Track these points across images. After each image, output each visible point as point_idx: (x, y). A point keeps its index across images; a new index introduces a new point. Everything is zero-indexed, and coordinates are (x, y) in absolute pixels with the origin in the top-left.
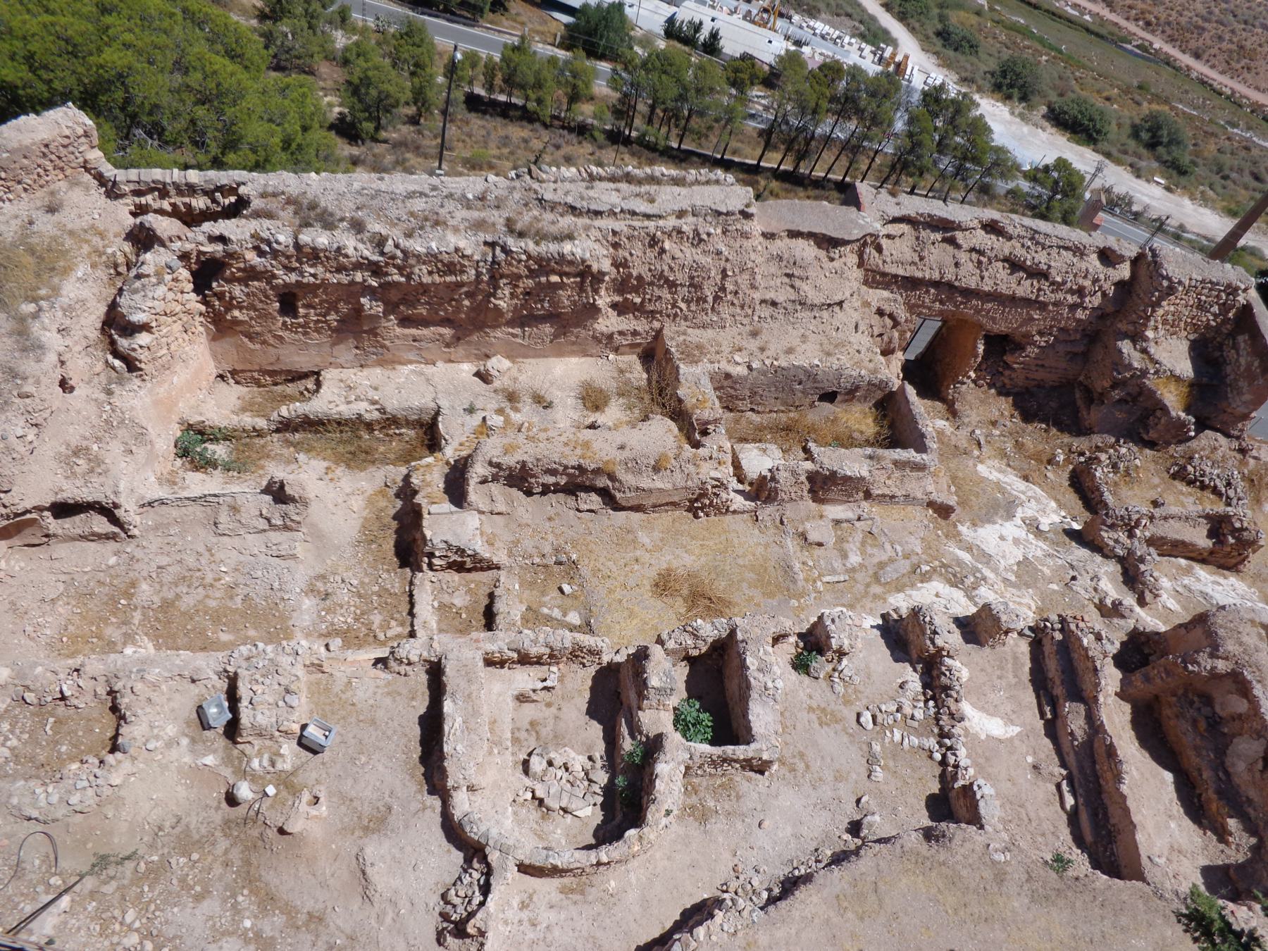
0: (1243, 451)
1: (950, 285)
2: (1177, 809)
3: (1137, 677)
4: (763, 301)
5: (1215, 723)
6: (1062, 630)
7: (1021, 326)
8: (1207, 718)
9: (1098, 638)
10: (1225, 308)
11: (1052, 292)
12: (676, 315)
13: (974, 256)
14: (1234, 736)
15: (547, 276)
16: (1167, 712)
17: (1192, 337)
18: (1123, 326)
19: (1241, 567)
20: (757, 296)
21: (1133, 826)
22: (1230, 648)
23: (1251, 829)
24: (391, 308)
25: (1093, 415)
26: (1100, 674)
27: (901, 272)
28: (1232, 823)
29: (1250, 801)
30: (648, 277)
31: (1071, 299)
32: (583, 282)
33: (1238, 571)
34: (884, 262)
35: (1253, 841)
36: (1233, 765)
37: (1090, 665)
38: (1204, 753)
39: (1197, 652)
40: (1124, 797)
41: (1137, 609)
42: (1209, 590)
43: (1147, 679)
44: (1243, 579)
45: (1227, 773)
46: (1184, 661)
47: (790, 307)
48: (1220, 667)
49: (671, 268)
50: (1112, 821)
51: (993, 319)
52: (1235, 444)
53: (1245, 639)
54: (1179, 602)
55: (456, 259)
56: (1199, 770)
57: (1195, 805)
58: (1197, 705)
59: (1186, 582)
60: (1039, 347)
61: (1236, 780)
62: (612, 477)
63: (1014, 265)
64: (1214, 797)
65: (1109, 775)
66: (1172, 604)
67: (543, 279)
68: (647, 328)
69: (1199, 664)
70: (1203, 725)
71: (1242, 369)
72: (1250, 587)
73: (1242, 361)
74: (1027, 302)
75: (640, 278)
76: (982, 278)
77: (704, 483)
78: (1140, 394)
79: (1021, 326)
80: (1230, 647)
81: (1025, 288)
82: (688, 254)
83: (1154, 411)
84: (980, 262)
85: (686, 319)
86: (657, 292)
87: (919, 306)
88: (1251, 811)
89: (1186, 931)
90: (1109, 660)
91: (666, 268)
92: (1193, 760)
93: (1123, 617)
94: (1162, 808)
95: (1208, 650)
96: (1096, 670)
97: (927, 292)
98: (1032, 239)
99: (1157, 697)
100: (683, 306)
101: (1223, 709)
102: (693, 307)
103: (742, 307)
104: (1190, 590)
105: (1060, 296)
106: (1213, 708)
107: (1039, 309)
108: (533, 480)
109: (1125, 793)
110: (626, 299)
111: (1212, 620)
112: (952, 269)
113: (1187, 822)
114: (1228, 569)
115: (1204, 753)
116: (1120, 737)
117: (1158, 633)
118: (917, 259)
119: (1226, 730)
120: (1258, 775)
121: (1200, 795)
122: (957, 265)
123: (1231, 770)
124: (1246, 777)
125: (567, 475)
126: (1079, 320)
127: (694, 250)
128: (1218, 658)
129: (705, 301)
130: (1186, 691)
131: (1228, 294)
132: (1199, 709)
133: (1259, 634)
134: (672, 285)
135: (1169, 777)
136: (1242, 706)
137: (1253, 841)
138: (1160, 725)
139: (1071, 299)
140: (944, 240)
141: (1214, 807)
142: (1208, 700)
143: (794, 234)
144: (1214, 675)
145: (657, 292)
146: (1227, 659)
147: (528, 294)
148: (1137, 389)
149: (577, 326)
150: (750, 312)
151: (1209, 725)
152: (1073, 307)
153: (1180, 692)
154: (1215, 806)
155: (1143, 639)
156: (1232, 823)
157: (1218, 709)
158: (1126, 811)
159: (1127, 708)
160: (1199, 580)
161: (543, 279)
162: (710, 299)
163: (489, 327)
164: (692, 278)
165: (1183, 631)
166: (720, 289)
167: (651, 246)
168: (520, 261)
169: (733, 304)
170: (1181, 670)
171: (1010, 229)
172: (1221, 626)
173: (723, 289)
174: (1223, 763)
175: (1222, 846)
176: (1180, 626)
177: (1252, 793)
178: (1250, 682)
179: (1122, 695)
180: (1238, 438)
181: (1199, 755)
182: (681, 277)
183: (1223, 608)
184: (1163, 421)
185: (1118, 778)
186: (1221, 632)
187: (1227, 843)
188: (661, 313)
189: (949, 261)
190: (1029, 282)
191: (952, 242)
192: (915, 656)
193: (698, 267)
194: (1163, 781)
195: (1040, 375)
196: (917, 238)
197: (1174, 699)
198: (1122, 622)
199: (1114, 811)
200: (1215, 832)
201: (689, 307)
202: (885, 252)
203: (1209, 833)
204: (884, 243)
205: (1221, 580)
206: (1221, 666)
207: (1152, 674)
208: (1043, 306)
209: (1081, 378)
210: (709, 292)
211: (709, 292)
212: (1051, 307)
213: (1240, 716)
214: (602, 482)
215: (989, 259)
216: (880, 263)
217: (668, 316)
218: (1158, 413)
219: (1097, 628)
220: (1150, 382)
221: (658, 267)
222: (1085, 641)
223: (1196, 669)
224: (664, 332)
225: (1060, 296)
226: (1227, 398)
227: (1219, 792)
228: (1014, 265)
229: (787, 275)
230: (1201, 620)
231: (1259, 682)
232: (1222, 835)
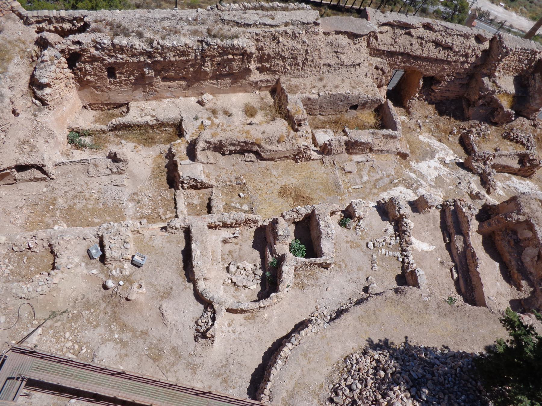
0: (535, 126)
1: (408, 55)
2: (500, 277)
3: (485, 224)
4: (324, 64)
5: (517, 242)
6: (454, 205)
7: (439, 72)
8: (514, 240)
9: (470, 208)
10: (530, 61)
11: (454, 56)
12: (285, 72)
13: (419, 40)
14: (525, 247)
15: (227, 56)
16: (498, 238)
17: (515, 75)
18: (485, 71)
19: (532, 176)
20: (322, 62)
21: (482, 285)
22: (526, 210)
23: (531, 284)
24: (158, 73)
25: (470, 112)
26: (470, 223)
27: (386, 49)
28: (523, 282)
29: (531, 273)
30: (272, 55)
31: (462, 59)
32: (243, 58)
33: (530, 178)
34: (379, 44)
35: (532, 289)
36: (525, 259)
37: (466, 219)
38: (513, 254)
39: (511, 212)
40: (478, 273)
41: (487, 195)
42: (517, 187)
43: (490, 224)
44: (532, 181)
45: (522, 263)
46: (506, 217)
47: (337, 67)
48: (521, 218)
49: (283, 50)
50: (473, 283)
51: (427, 70)
52: (532, 123)
53: (532, 206)
54: (504, 192)
55: (186, 49)
56: (510, 261)
57: (508, 276)
58: (510, 235)
59: (508, 183)
60: (447, 82)
61: (526, 265)
62: (259, 146)
63: (437, 44)
64: (516, 272)
65: (473, 265)
66: (501, 193)
67: (225, 57)
68: (273, 78)
69: (512, 218)
70: (512, 243)
71: (536, 89)
72: (535, 185)
73: (537, 85)
74: (442, 61)
75: (269, 55)
76: (423, 50)
77: (300, 147)
78: (491, 101)
79: (439, 72)
80: (526, 210)
81: (442, 55)
82: (290, 43)
83: (497, 109)
84: (422, 43)
85: (290, 74)
86: (277, 62)
87: (394, 65)
88: (531, 277)
89: (504, 326)
90: (474, 217)
91: (280, 50)
92: (508, 257)
93: (480, 199)
94: (494, 277)
95: (516, 211)
96: (468, 221)
97: (398, 58)
98: (445, 31)
99: (493, 232)
100: (289, 68)
101: (521, 236)
102: (293, 68)
103: (315, 67)
104: (509, 187)
105: (457, 58)
106: (517, 235)
107: (448, 64)
108: (225, 149)
109: (479, 271)
110: (263, 65)
111: (518, 199)
112: (409, 47)
113: (504, 283)
114: (526, 177)
115: (513, 254)
116: (477, 249)
117: (495, 205)
118: (393, 43)
119: (522, 245)
120: (535, 263)
121: (510, 271)
122: (411, 45)
123: (524, 261)
124: (530, 263)
125: (240, 146)
126: (465, 69)
127: (293, 42)
128: (520, 215)
129: (298, 65)
130: (506, 229)
131: (532, 55)
132: (511, 236)
133: (538, 204)
134: (284, 58)
135: (497, 264)
136: (530, 234)
137: (532, 289)
138: (494, 244)
139: (462, 59)
140: (406, 33)
141: (516, 276)
142: (515, 232)
143: (338, 33)
144: (518, 222)
145: (277, 62)
146: (524, 215)
147: (219, 64)
148: (490, 99)
149: (242, 78)
150: (319, 69)
151: (515, 243)
152: (463, 63)
153: (503, 230)
154: (516, 276)
155: (488, 208)
156: (523, 282)
157: (519, 236)
158: (479, 279)
159: (481, 237)
160: (513, 182)
161: (225, 57)
162: (301, 64)
163: (202, 80)
164: (292, 54)
165: (506, 204)
166: (305, 59)
167: (273, 40)
168: (214, 49)
169: (311, 66)
170: (504, 220)
171: (435, 27)
172: (522, 202)
173: (306, 59)
174: (520, 258)
175: (519, 292)
176: (505, 202)
177: (532, 270)
178: (534, 225)
179: (479, 232)
180: (533, 120)
181: (510, 255)
182: (287, 54)
183: (524, 193)
184: (501, 113)
185: (476, 266)
186: (522, 204)
187: (521, 291)
188: (279, 71)
189: (408, 43)
190: (444, 51)
191: (409, 34)
192: (391, 218)
193: (295, 49)
194: (495, 266)
195: (447, 94)
196: (394, 33)
197: (501, 232)
198: (480, 201)
199: (474, 279)
200: (516, 286)
201: (291, 68)
202: (379, 40)
203: (513, 287)
204: (379, 35)
205: (523, 182)
206: (522, 218)
207: (492, 223)
208: (449, 63)
209: (465, 95)
210: (300, 61)
211: (300, 61)
212: (453, 63)
213: (529, 238)
214: (255, 148)
215: (426, 42)
216: (377, 45)
217: (282, 73)
218: (499, 110)
219: (469, 204)
220: (496, 96)
221: (277, 50)
222: (464, 210)
223: (511, 220)
224: (281, 80)
225: (457, 58)
226: (529, 102)
227: (518, 270)
228: (437, 44)
229: (335, 52)
230: (514, 199)
231: (537, 224)
232: (519, 287)
